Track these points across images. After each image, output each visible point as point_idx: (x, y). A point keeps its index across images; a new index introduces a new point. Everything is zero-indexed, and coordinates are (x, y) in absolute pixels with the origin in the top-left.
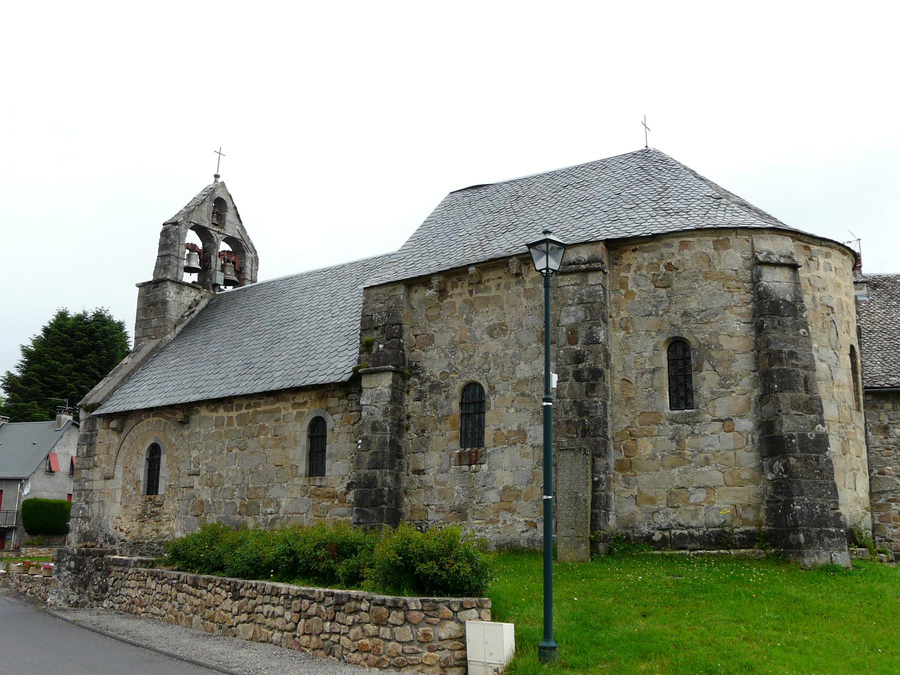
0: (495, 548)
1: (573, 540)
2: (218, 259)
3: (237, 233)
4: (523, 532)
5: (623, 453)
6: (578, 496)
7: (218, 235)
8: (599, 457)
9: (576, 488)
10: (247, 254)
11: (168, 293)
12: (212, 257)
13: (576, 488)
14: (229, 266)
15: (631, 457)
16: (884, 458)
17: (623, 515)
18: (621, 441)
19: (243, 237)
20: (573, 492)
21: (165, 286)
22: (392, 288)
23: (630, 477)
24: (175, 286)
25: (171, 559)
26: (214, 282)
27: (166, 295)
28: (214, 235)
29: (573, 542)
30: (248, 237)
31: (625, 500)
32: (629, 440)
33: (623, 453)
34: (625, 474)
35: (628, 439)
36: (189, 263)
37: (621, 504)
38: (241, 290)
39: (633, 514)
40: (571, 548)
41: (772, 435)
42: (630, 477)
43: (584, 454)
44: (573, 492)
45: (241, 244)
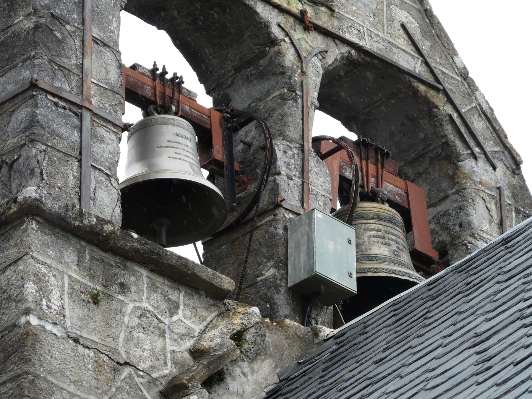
0: (289, 124)
2: (313, 163)
3: (403, 42)
7: (298, 34)
10: (468, 164)
11: (31, 288)
12: (279, 146)
14: (378, 217)
19: (440, 69)
21: (13, 253)
22: (517, 360)
24: (71, 256)
26: (303, 276)
27: (20, 299)
28: (276, 31)
30: (464, 75)
36: (150, 166)
38: (409, 296)
41: (263, 277)
45: (431, 106)
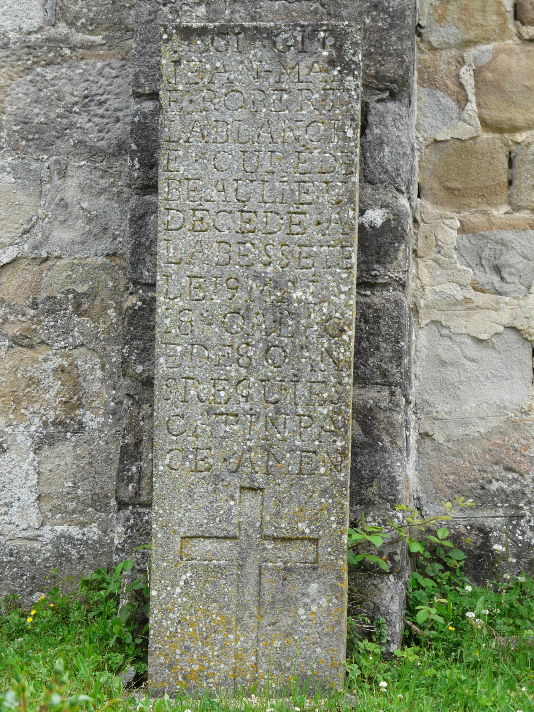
1: (254, 556)
4: (476, 455)
5: (472, 106)
6: (286, 300)
8: (393, 96)
9: (275, 252)
13: (275, 252)
15: (515, 129)
16: (375, 81)
17: (458, 432)
18: (467, 44)
20: (257, 276)
23: (508, 235)
25: (113, 423)
29: (251, 568)
31: (473, 350)
32: (512, 43)
33: (472, 106)
34: (477, 219)
35: (502, 34)
37: (451, 374)
39: (515, 425)
40: (242, 606)
42: (508, 235)
43: (332, 63)
44: (257, 276)
